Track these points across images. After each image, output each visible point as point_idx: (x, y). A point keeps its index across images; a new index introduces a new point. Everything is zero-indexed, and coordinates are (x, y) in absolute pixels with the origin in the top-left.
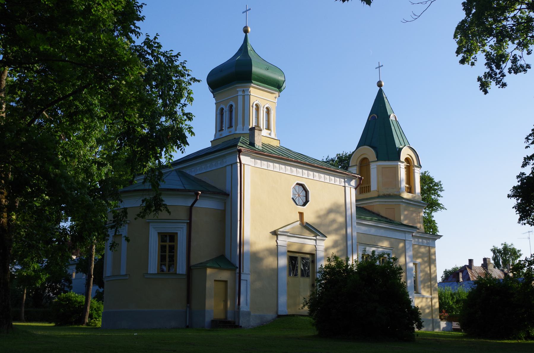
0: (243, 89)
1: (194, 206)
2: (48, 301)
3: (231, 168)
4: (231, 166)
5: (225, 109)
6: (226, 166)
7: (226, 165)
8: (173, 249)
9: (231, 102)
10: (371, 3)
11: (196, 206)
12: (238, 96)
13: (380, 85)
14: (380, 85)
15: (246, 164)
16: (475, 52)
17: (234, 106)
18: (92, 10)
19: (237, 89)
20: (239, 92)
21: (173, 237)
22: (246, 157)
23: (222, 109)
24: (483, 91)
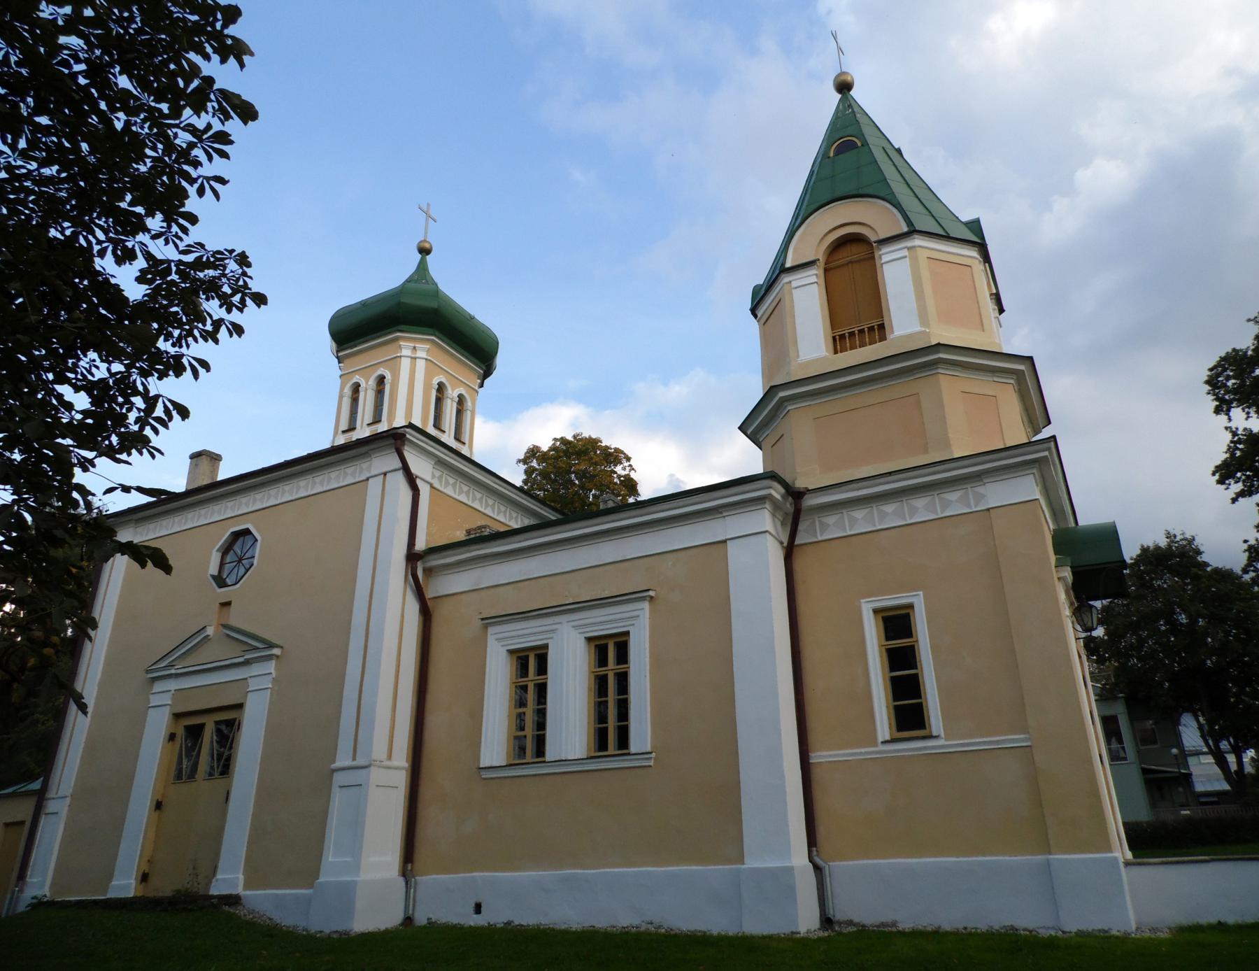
0: (413, 345)
1: (796, 543)
2: (1211, 661)
3: (382, 480)
4: (382, 476)
5: (363, 384)
6: (368, 479)
7: (368, 475)
8: (623, 680)
9: (358, 377)
10: (73, 391)
11: (803, 542)
12: (400, 357)
13: (844, 87)
14: (844, 87)
15: (419, 478)
16: (263, 916)
17: (388, 377)
18: (9, 486)
19: (401, 343)
20: (403, 350)
21: (622, 645)
22: (239, 474)
23: (356, 388)
24: (1208, 376)
